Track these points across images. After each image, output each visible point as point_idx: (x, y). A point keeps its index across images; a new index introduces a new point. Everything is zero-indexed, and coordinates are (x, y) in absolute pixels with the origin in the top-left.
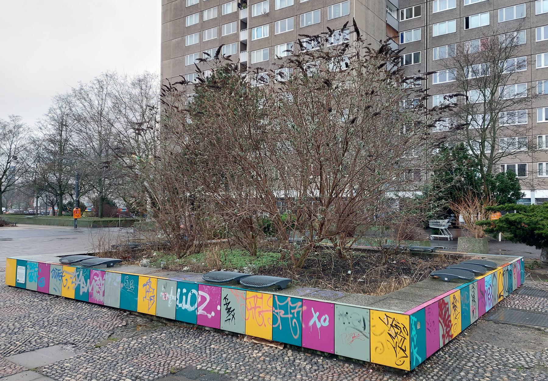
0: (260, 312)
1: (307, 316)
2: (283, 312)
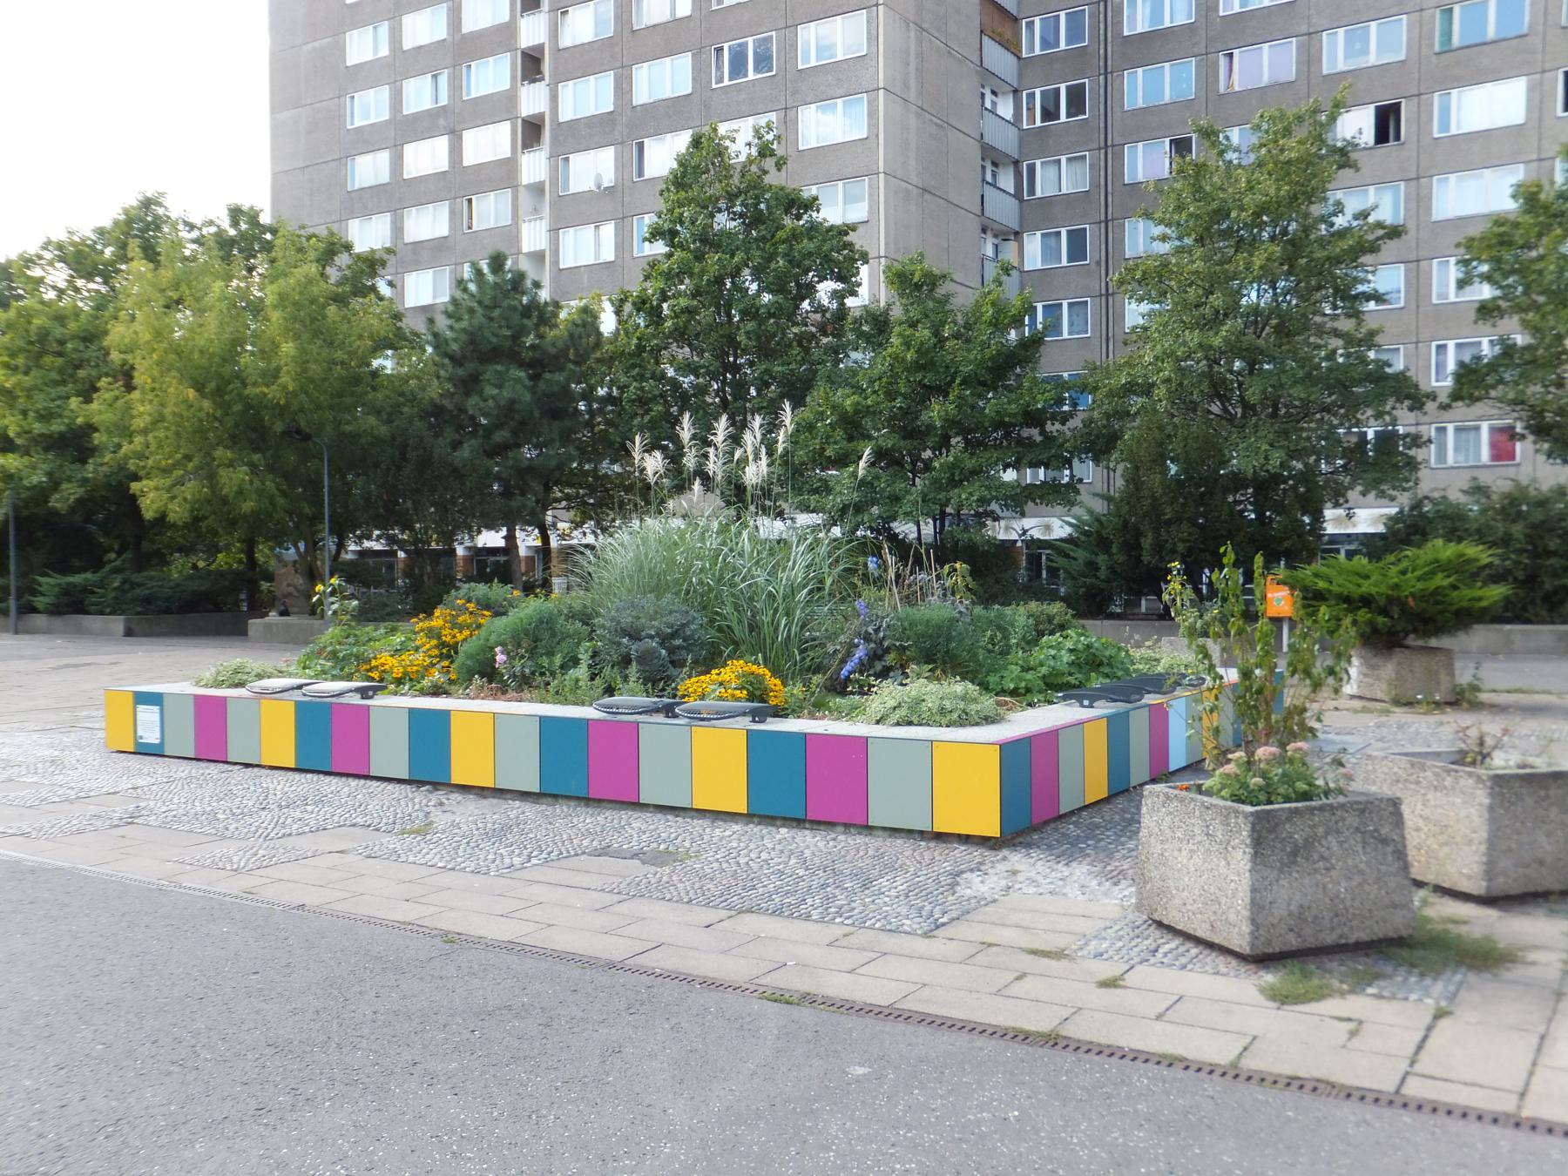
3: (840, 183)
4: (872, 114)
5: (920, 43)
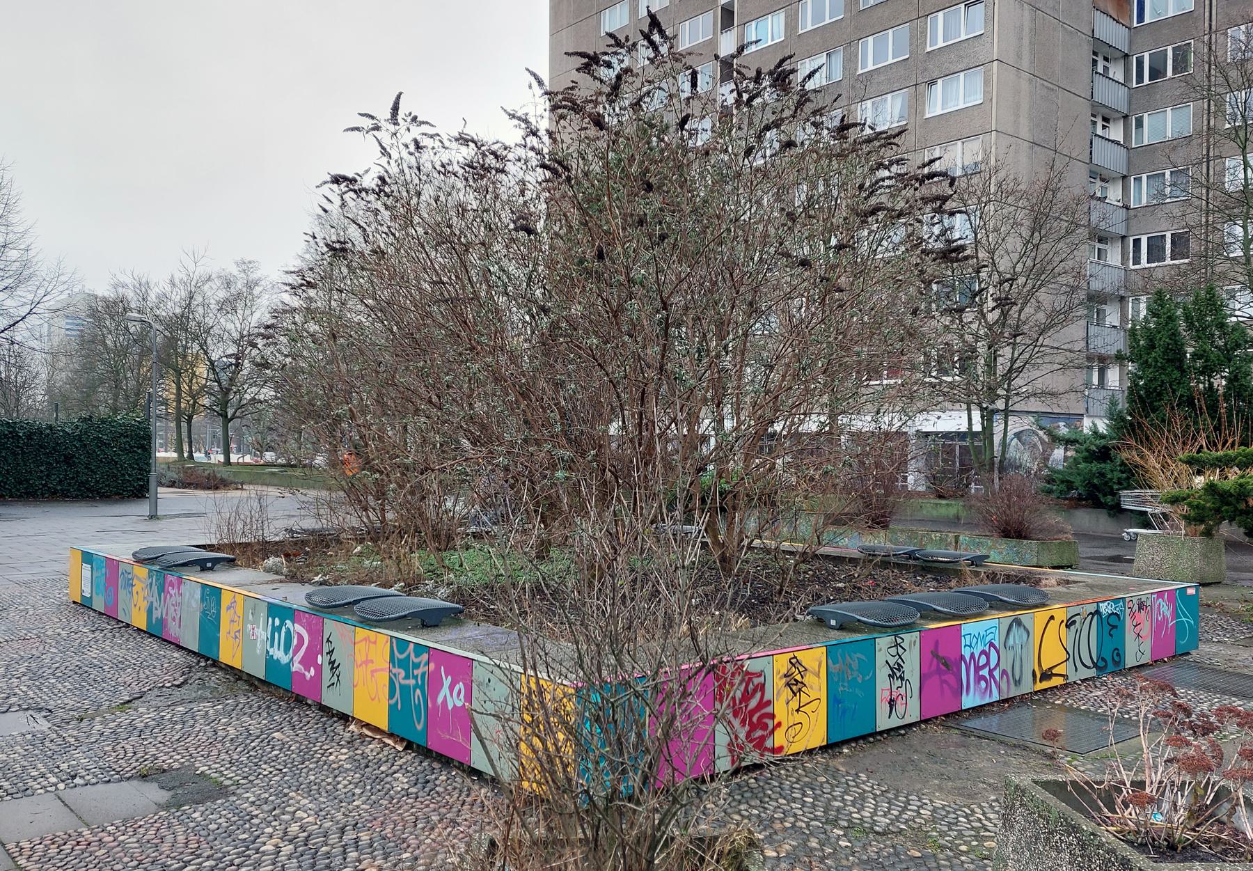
0: (373, 672)
1: (434, 684)
2: (403, 673)
3: (959, 143)
4: (987, 82)
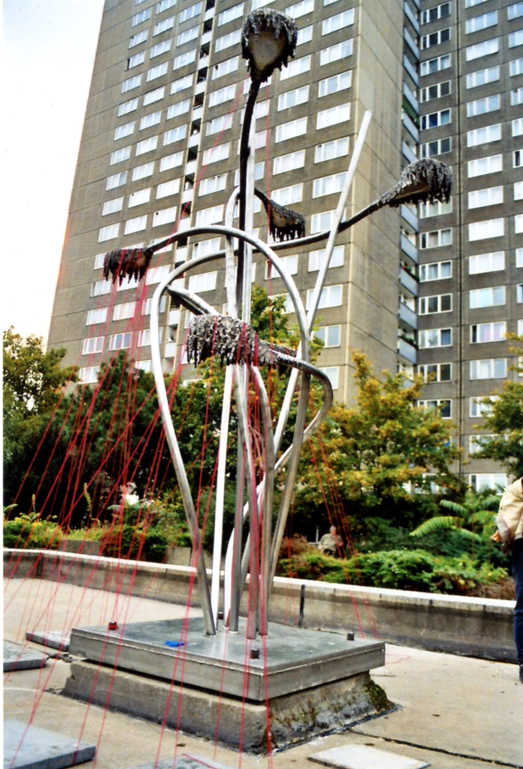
4: (345, 294)
5: (370, 264)
